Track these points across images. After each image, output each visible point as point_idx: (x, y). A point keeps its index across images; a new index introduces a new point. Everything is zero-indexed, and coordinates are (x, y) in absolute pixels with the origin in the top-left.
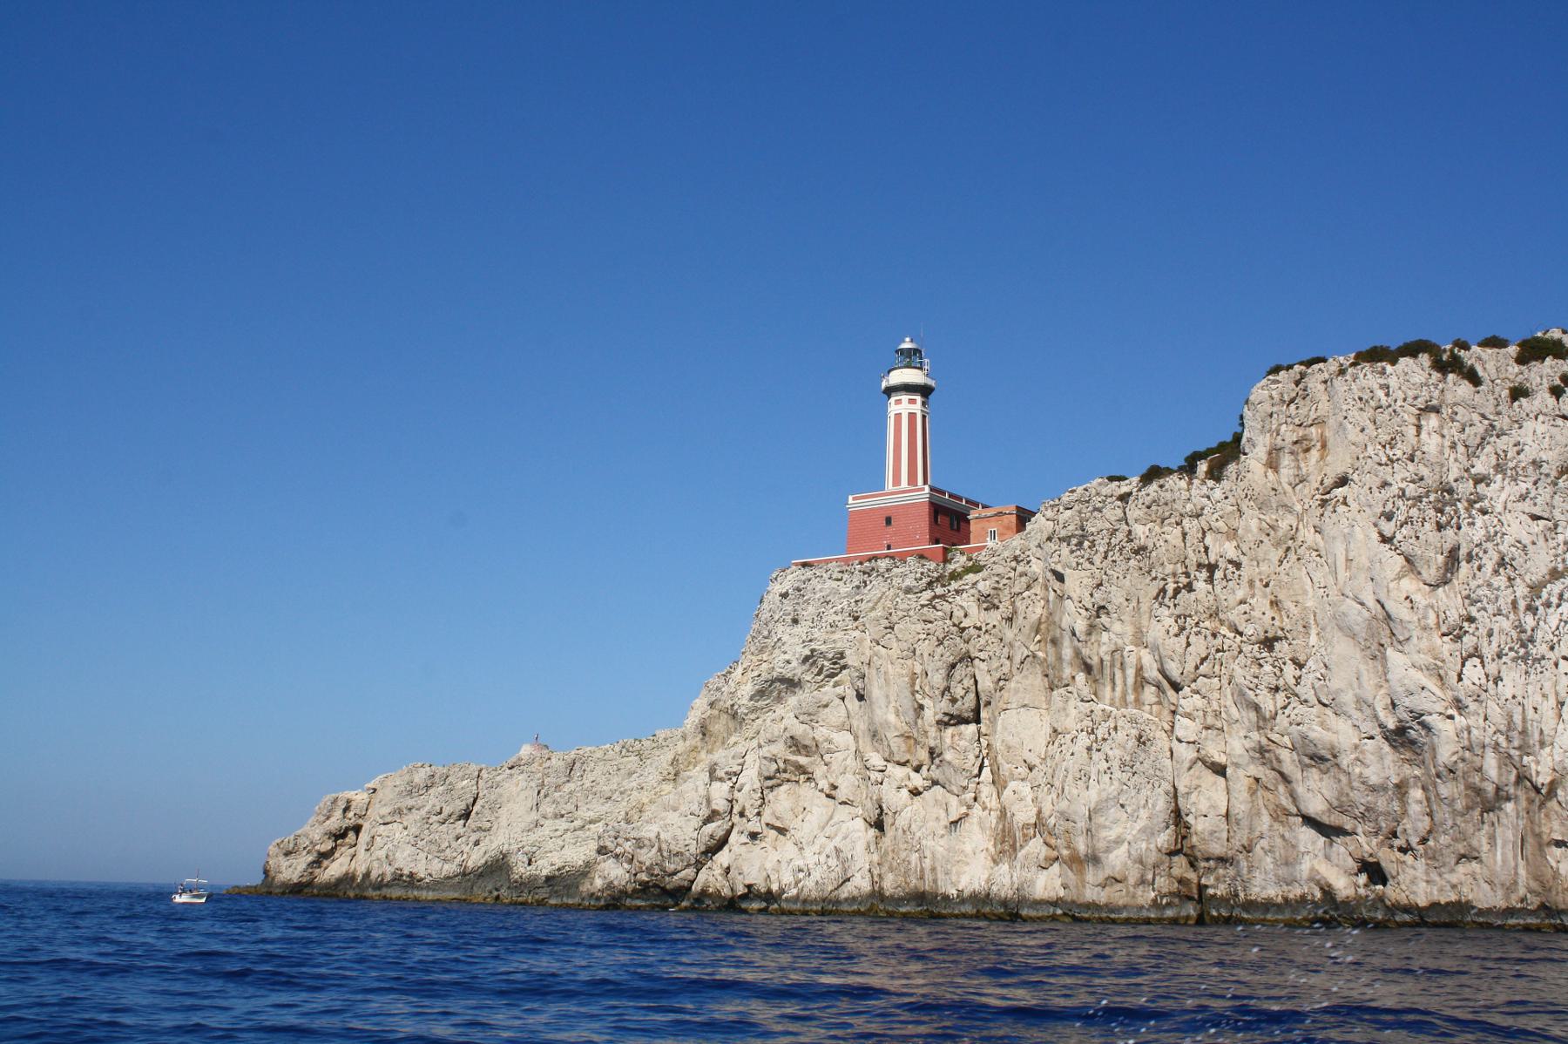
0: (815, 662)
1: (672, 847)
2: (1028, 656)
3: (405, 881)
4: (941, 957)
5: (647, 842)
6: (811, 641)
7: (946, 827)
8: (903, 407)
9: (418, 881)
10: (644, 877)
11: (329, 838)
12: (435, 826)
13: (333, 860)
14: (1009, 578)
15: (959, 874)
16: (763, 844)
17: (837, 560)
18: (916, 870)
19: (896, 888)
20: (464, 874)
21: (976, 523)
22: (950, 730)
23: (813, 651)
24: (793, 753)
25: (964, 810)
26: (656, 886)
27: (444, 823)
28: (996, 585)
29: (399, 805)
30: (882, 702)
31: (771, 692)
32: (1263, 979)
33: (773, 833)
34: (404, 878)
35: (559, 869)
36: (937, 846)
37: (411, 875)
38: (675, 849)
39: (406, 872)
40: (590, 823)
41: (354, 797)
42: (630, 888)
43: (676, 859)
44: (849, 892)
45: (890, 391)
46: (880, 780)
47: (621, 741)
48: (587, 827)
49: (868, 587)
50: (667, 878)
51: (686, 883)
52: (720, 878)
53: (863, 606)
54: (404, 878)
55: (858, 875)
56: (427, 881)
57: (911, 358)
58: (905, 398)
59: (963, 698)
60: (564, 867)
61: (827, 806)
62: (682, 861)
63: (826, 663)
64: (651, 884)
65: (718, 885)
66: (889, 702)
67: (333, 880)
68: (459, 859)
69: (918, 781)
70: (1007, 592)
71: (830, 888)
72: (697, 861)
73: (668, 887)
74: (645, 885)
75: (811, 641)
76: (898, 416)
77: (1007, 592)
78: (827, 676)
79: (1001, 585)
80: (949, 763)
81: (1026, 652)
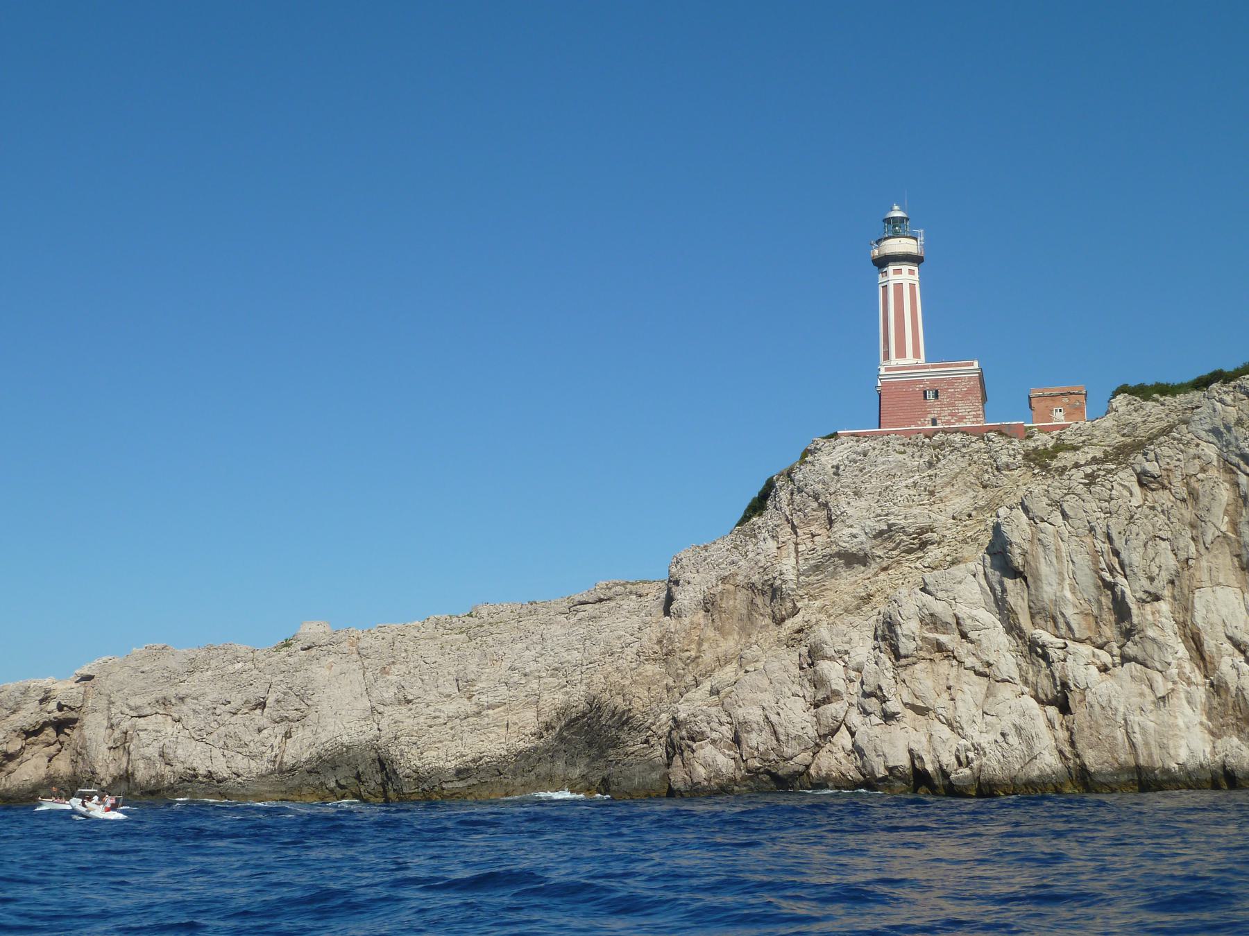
0: (890, 537)
1: (790, 731)
2: (1218, 536)
3: (201, 783)
4: (132, 824)
5: (755, 726)
6: (887, 515)
7: (1154, 703)
8: (905, 277)
9: (219, 782)
10: (756, 763)
11: (18, 736)
12: (227, 717)
13: (21, 763)
14: (1179, 460)
15: (1176, 747)
16: (903, 725)
17: (896, 433)
18: (1124, 745)
19: (1102, 764)
20: (281, 772)
21: (1038, 402)
22: (1148, 607)
23: (890, 526)
24: (930, 630)
25: (1170, 685)
26: (768, 772)
27: (235, 714)
28: (1168, 467)
29: (164, 693)
30: (1054, 579)
31: (828, 566)
32: (447, 813)
33: (910, 713)
34: (200, 778)
35: (474, 760)
36: (1147, 722)
37: (210, 775)
38: (793, 732)
39: (202, 771)
40: (488, 708)
41: (53, 687)
42: (738, 776)
43: (794, 742)
44: (1040, 769)
45: (882, 262)
46: (1062, 657)
47: (432, 618)
48: (484, 713)
49: (943, 462)
50: (782, 763)
51: (801, 768)
52: (844, 761)
53: (938, 481)
54: (200, 778)
55: (1046, 752)
56: (230, 783)
57: (895, 227)
58: (905, 268)
59: (1158, 575)
60: (481, 758)
61: (980, 684)
62: (799, 745)
63: (905, 538)
64: (762, 770)
65: (843, 769)
66: (1063, 580)
67: (28, 786)
68: (269, 754)
69: (1105, 657)
70: (1178, 473)
71: (1017, 767)
72: (817, 744)
73: (780, 773)
74: (755, 773)
75: (887, 515)
76: (899, 287)
77: (1178, 473)
78: (904, 552)
79: (1171, 467)
80: (1154, 640)
81: (1217, 533)
